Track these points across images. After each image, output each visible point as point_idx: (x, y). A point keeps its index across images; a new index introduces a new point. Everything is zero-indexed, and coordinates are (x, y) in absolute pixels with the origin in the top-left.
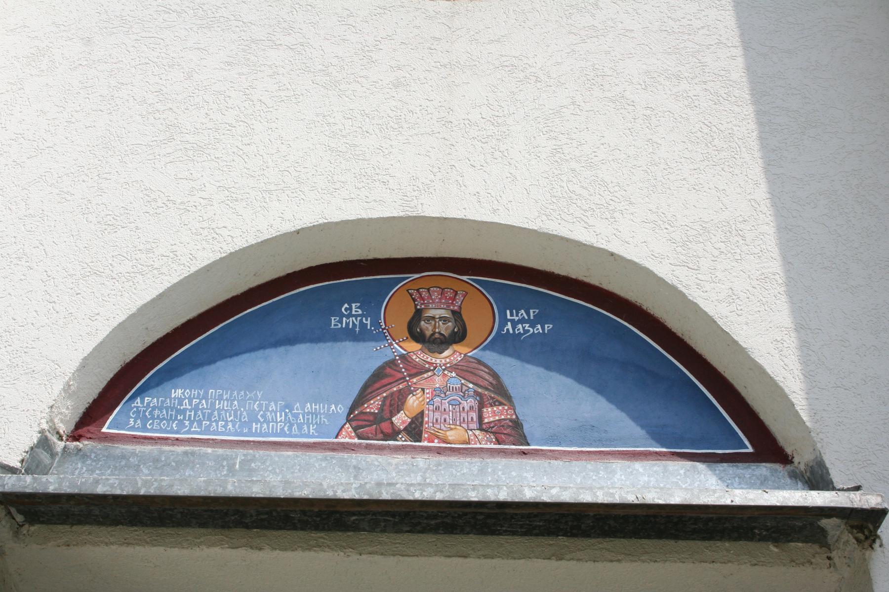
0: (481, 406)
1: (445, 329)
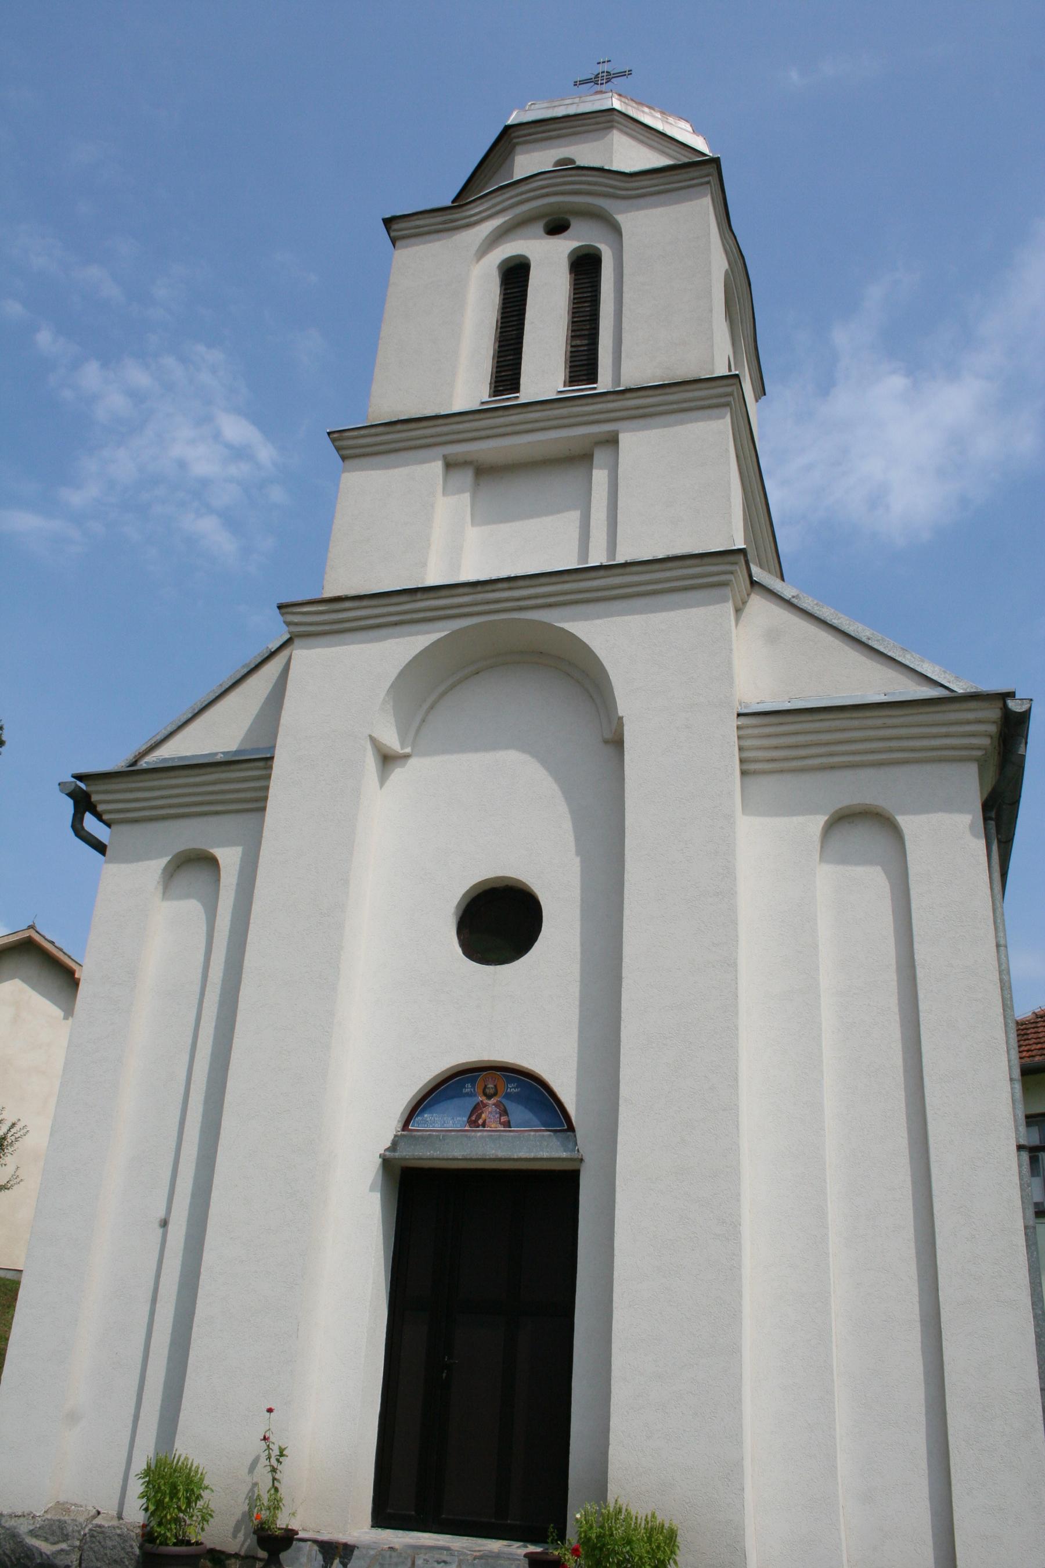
0: (501, 1116)
1: (492, 1091)
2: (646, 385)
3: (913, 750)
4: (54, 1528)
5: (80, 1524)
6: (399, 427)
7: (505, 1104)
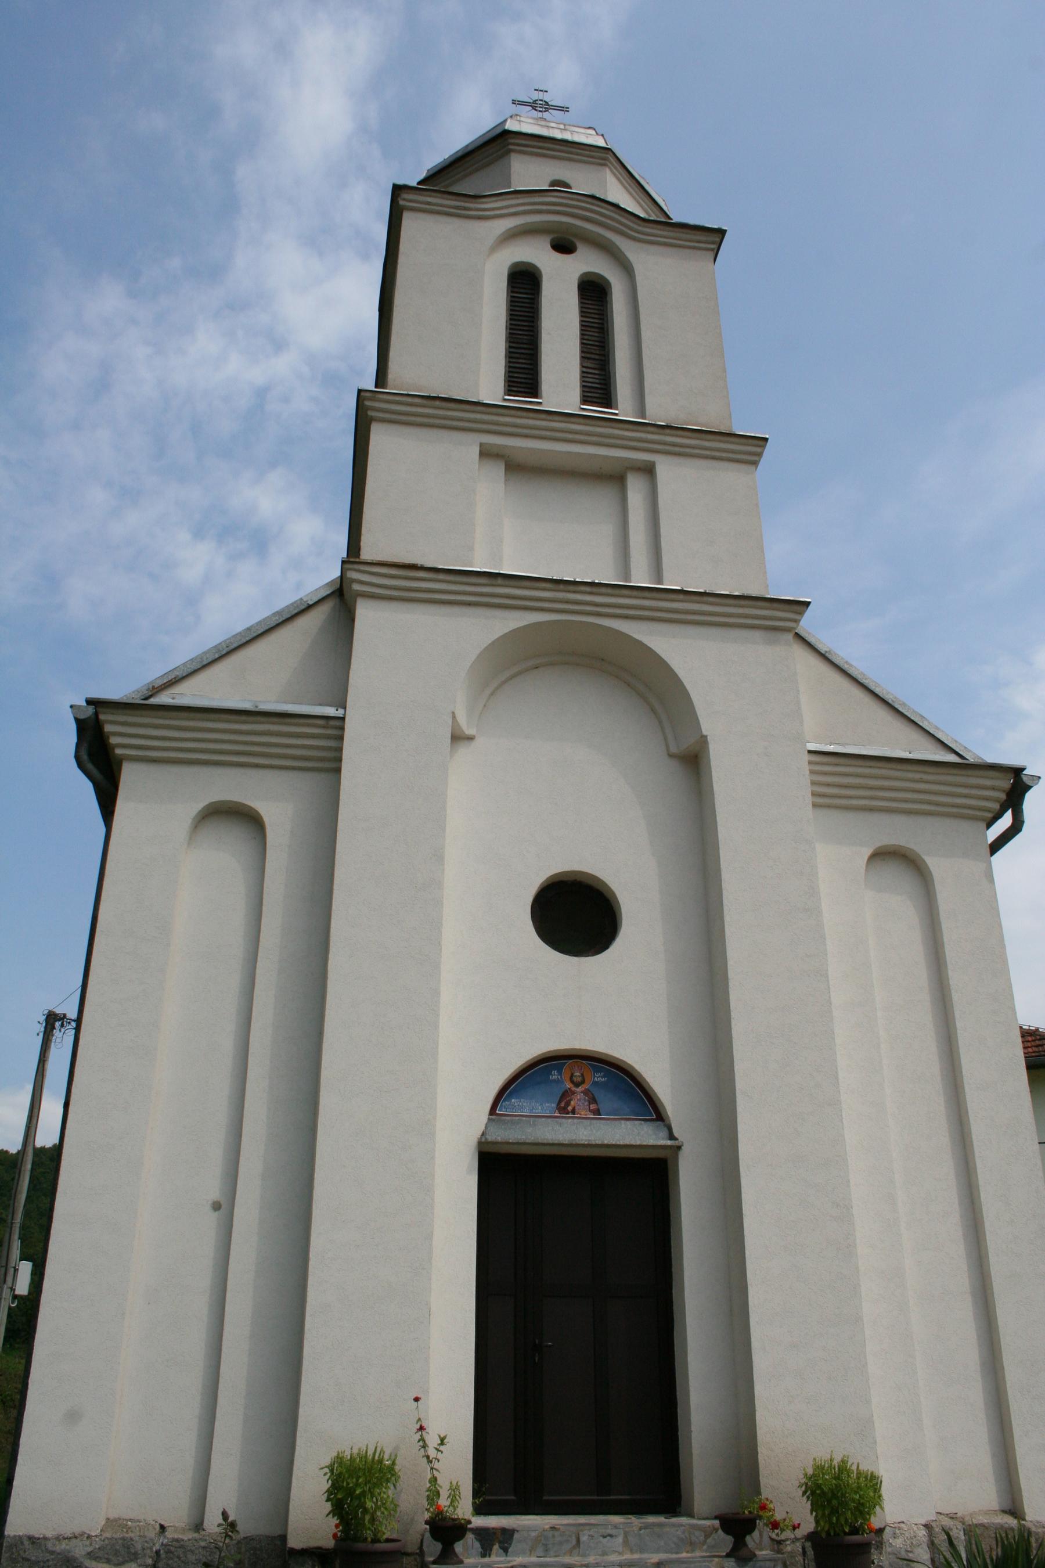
0: (590, 1104)
1: (579, 1079)
2: (685, 426)
3: (937, 804)
4: (118, 1548)
5: (151, 1540)
6: (437, 403)
7: (593, 1092)
